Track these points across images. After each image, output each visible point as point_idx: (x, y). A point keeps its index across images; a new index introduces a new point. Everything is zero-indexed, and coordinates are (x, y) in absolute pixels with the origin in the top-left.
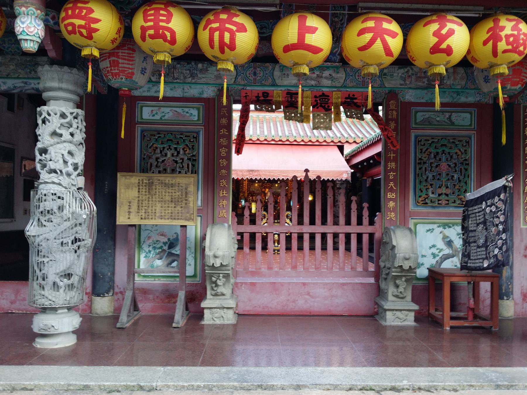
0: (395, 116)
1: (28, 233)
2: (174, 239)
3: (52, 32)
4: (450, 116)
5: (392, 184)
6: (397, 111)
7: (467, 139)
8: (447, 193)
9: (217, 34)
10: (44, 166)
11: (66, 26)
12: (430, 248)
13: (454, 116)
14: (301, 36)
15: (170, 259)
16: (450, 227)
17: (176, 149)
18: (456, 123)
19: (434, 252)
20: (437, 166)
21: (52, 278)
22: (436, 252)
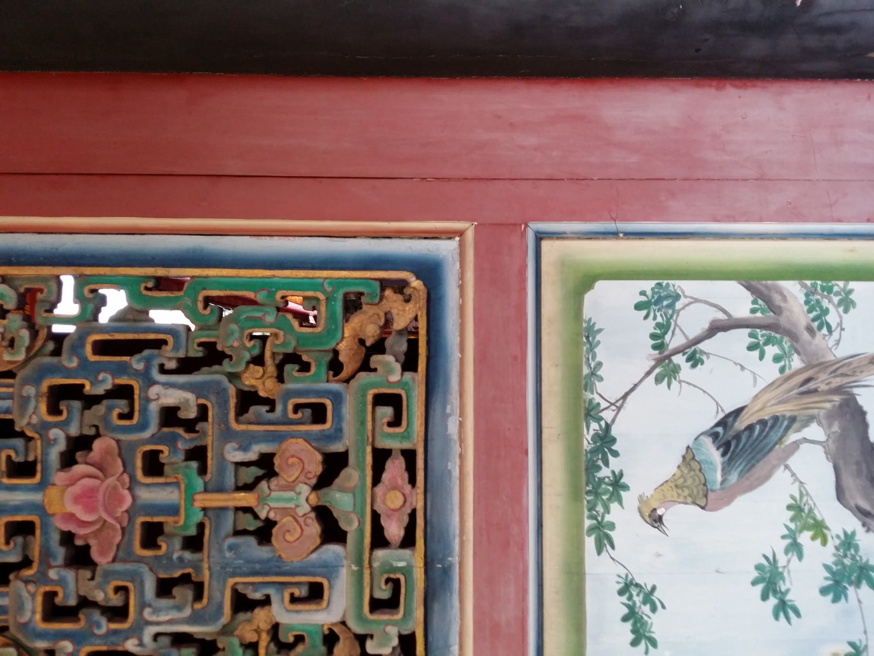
8: (315, 466)
12: (784, 608)
19: (821, 578)
20: (80, 557)
22: (818, 557)
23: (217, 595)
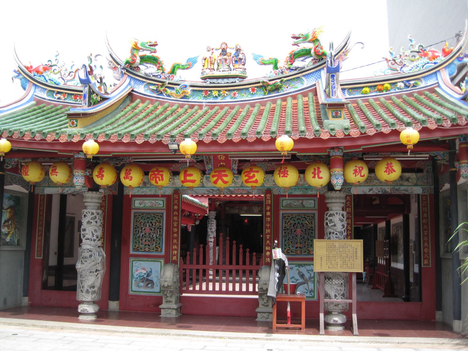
0: (270, 203)
1: (77, 267)
2: (150, 272)
4: (302, 202)
5: (268, 242)
6: (271, 200)
7: (313, 215)
13: (304, 202)
15: (147, 283)
16: (303, 266)
17: (151, 222)
18: (306, 206)
20: (295, 231)
23: (155, 151)
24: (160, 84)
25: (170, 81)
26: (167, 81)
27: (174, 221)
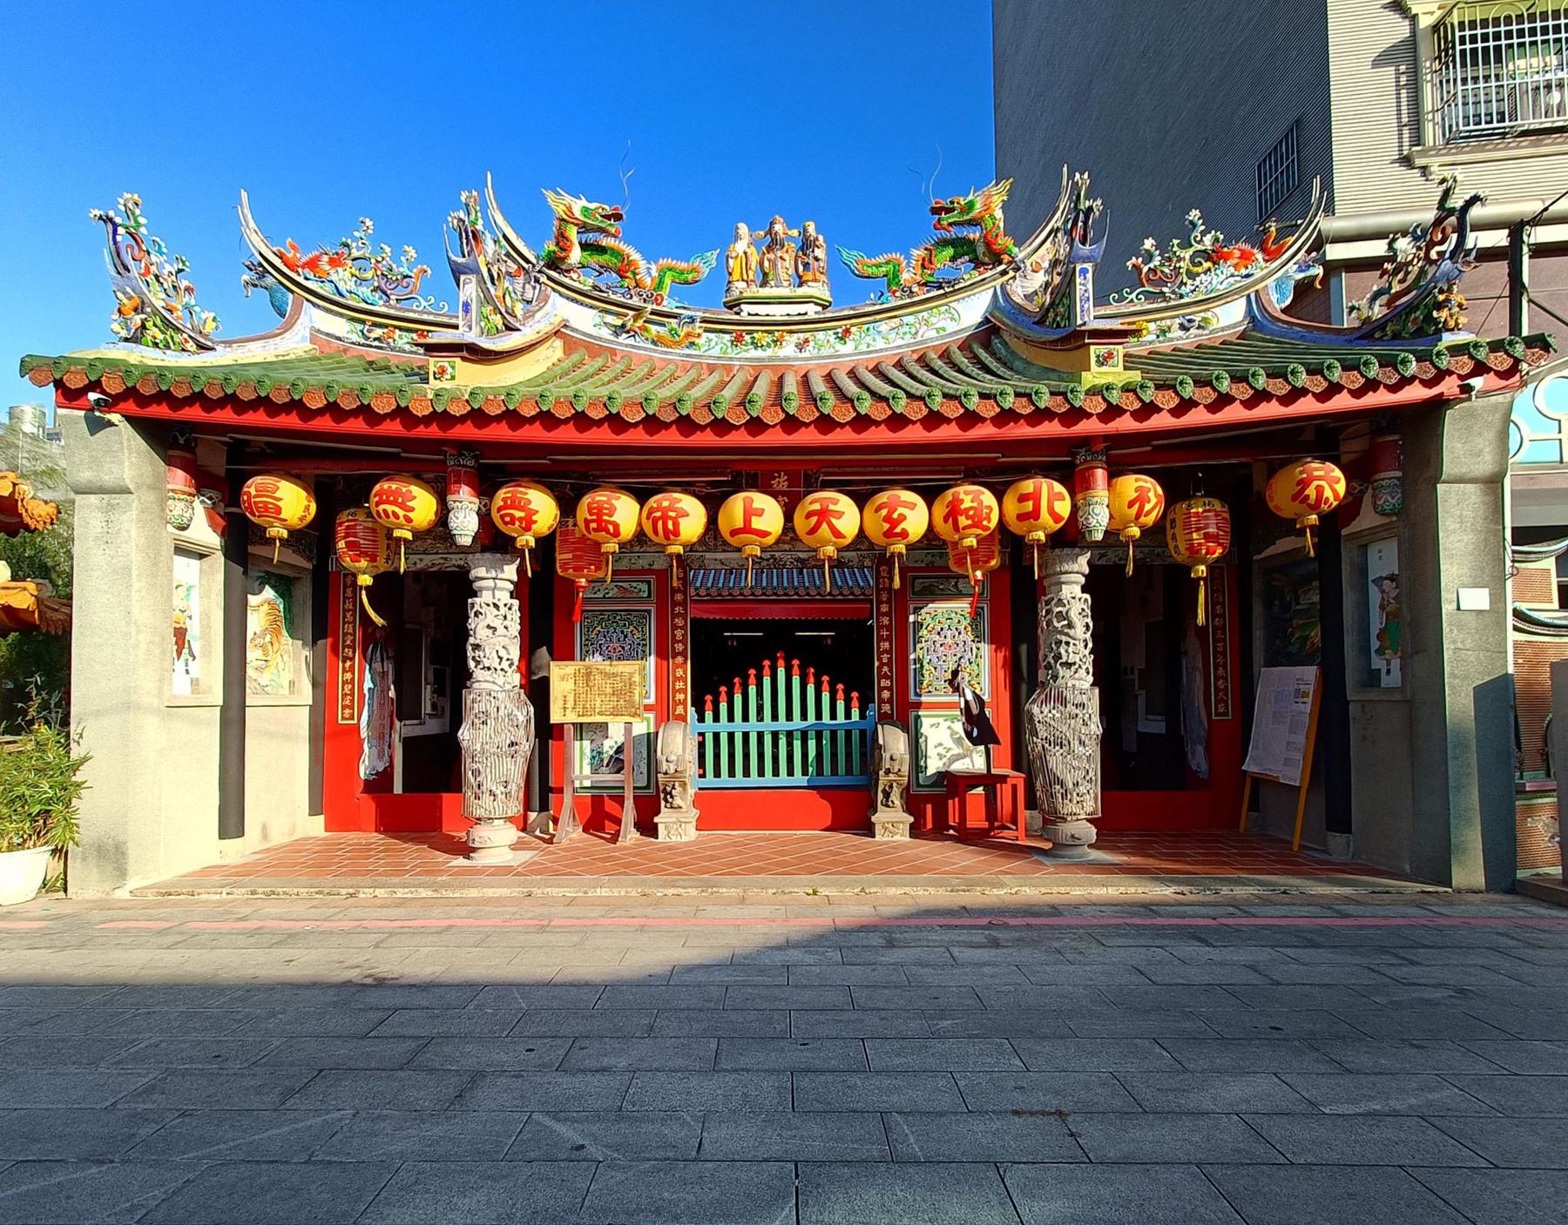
3: (485, 518)
5: (885, 669)
9: (660, 523)
10: (478, 663)
11: (502, 517)
14: (747, 521)
21: (489, 784)
22: (943, 752)
24: (631, 313)
25: (693, 769)
26: (650, 307)
27: (675, 627)
